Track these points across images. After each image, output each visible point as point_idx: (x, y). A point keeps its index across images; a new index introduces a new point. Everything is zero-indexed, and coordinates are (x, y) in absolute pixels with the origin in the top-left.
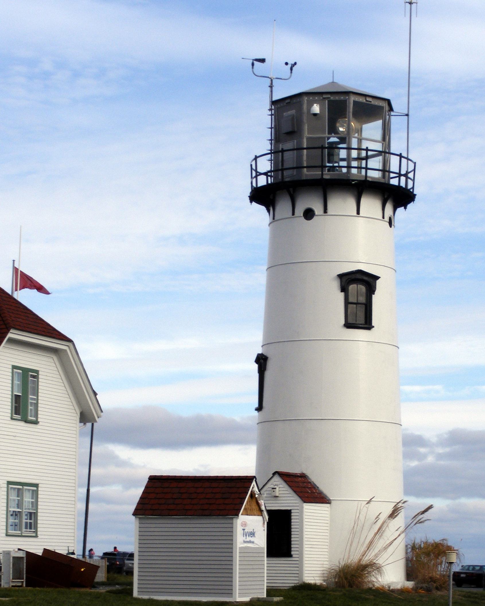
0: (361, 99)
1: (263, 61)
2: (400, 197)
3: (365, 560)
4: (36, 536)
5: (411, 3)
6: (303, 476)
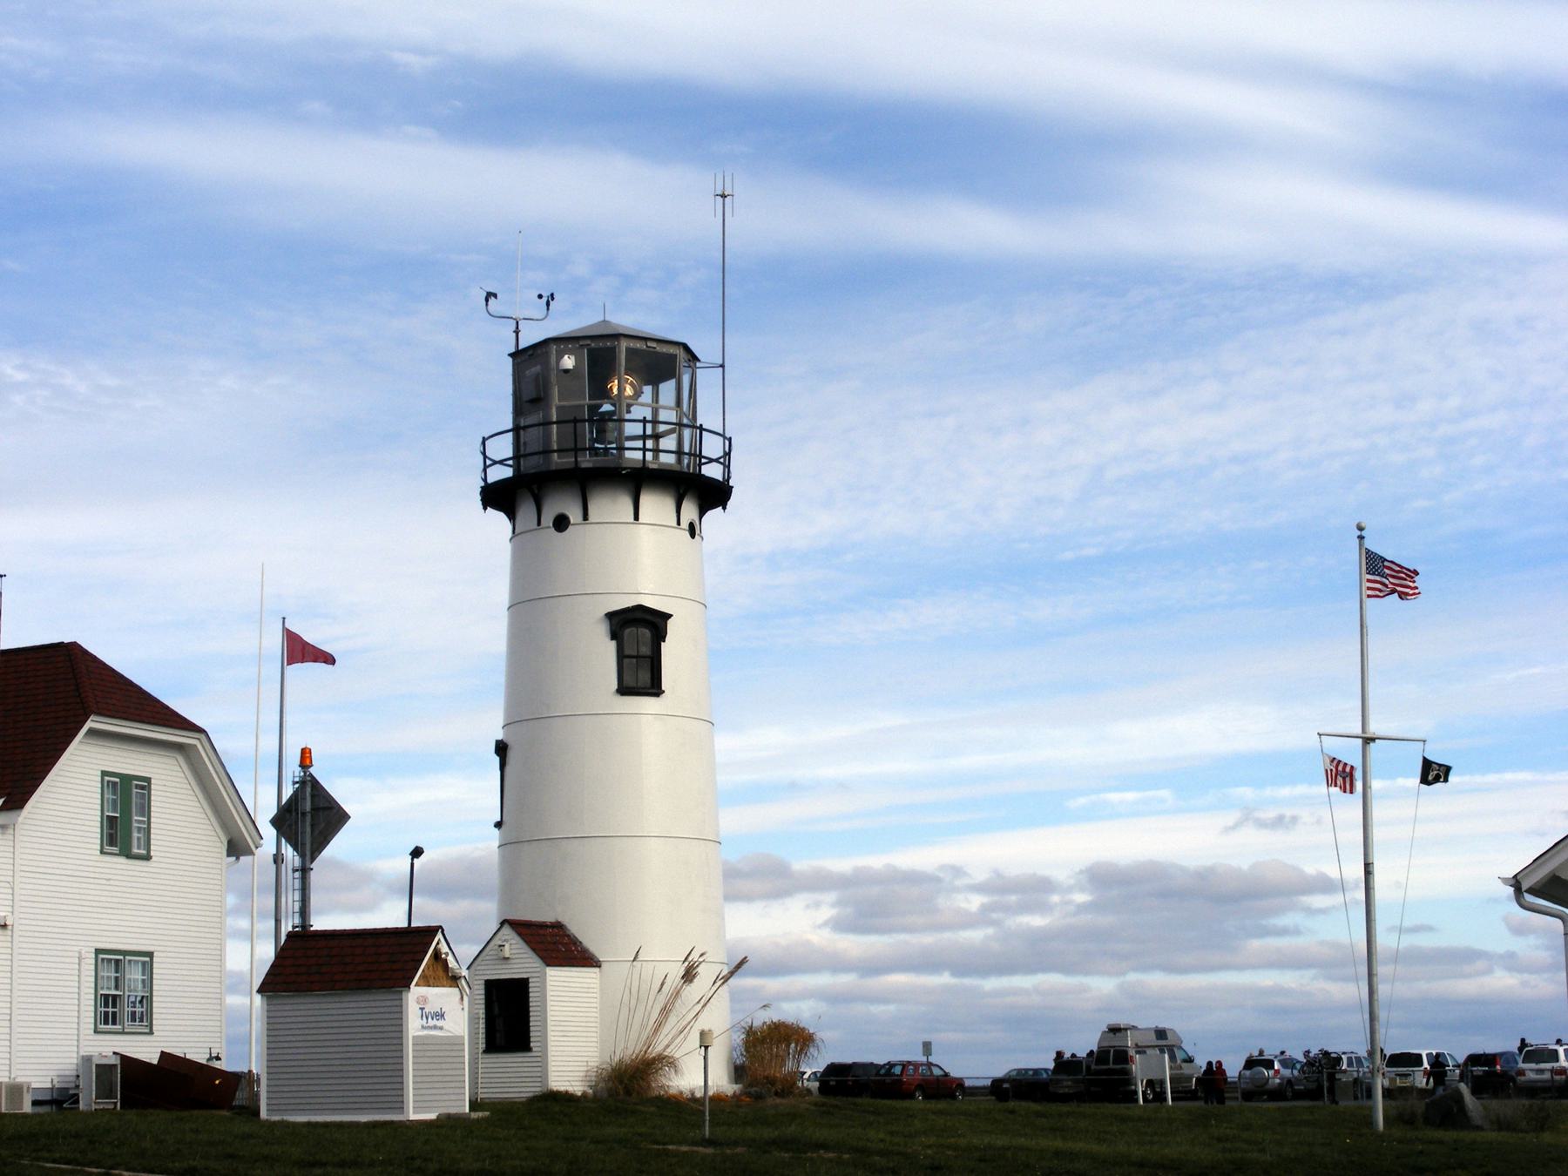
0: (639, 345)
3: (657, 1049)
4: (151, 1033)
5: (724, 196)
6: (558, 926)
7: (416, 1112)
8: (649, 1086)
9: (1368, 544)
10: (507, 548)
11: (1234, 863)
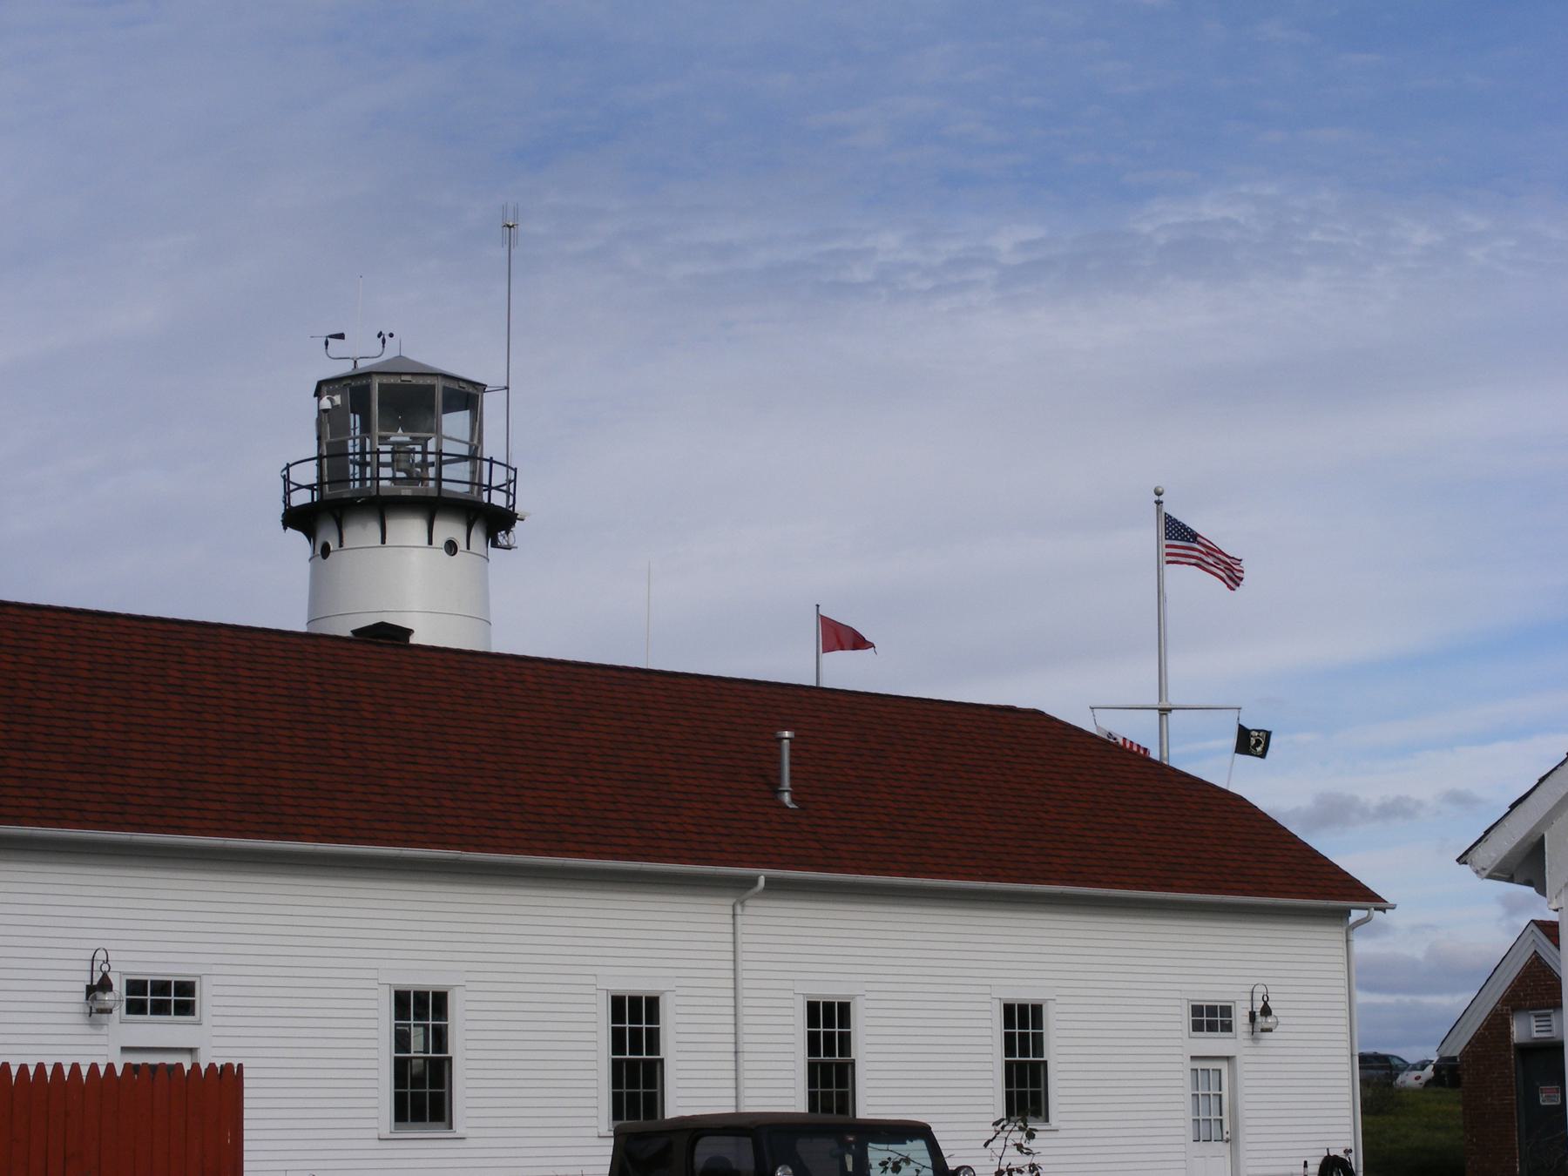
1: (341, 336)
2: (495, 522)
9: (1166, 508)
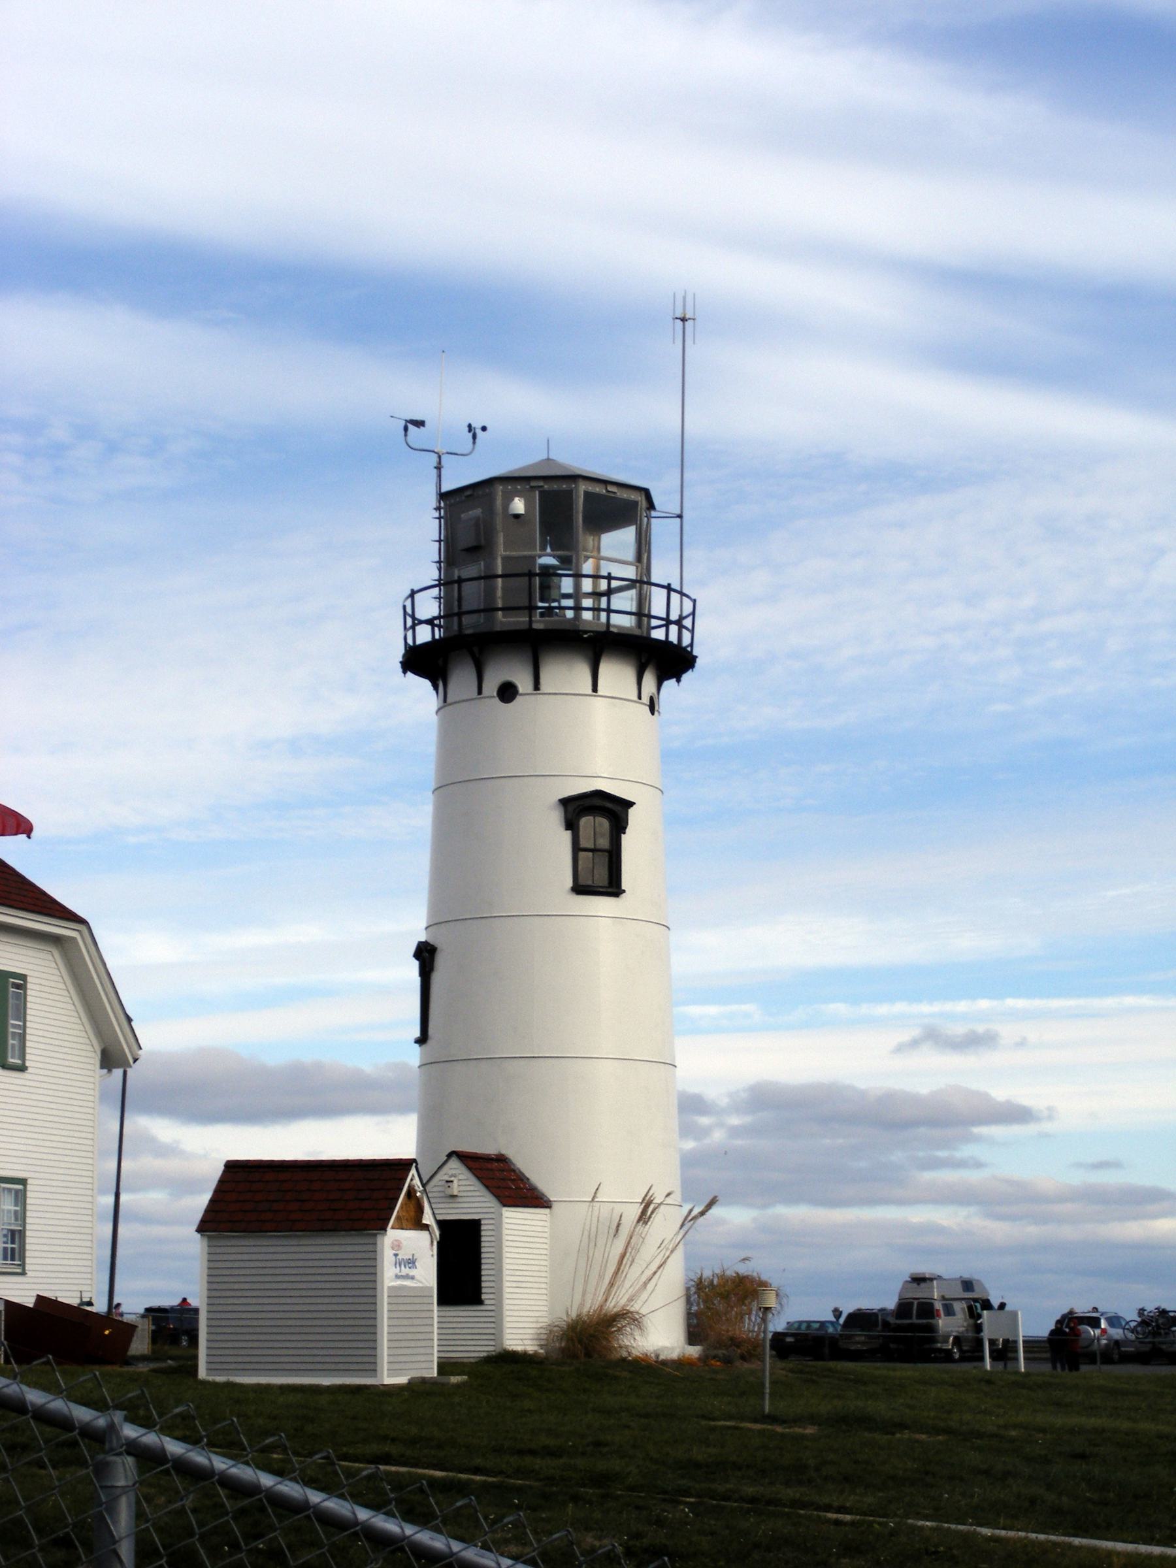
0: (598, 489)
4: (23, 1273)
5: (683, 320)
7: (391, 1375)
8: (610, 1349)
10: (434, 719)
11: (861, 1085)
